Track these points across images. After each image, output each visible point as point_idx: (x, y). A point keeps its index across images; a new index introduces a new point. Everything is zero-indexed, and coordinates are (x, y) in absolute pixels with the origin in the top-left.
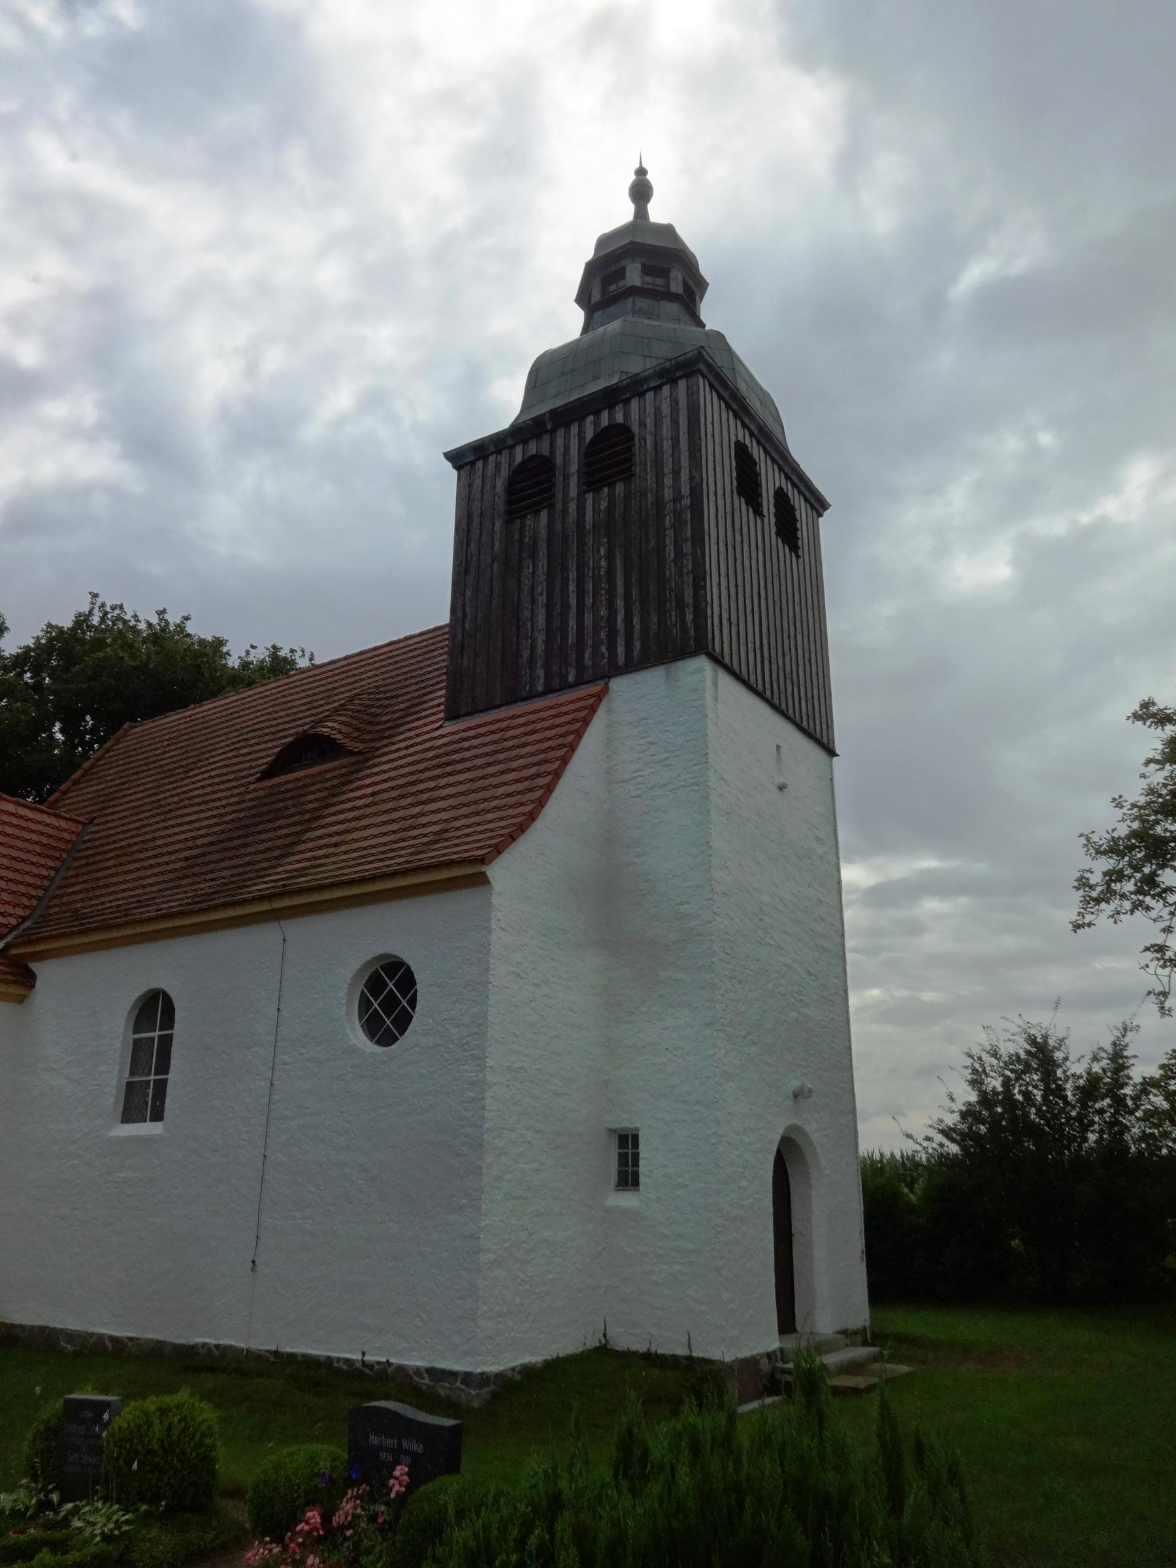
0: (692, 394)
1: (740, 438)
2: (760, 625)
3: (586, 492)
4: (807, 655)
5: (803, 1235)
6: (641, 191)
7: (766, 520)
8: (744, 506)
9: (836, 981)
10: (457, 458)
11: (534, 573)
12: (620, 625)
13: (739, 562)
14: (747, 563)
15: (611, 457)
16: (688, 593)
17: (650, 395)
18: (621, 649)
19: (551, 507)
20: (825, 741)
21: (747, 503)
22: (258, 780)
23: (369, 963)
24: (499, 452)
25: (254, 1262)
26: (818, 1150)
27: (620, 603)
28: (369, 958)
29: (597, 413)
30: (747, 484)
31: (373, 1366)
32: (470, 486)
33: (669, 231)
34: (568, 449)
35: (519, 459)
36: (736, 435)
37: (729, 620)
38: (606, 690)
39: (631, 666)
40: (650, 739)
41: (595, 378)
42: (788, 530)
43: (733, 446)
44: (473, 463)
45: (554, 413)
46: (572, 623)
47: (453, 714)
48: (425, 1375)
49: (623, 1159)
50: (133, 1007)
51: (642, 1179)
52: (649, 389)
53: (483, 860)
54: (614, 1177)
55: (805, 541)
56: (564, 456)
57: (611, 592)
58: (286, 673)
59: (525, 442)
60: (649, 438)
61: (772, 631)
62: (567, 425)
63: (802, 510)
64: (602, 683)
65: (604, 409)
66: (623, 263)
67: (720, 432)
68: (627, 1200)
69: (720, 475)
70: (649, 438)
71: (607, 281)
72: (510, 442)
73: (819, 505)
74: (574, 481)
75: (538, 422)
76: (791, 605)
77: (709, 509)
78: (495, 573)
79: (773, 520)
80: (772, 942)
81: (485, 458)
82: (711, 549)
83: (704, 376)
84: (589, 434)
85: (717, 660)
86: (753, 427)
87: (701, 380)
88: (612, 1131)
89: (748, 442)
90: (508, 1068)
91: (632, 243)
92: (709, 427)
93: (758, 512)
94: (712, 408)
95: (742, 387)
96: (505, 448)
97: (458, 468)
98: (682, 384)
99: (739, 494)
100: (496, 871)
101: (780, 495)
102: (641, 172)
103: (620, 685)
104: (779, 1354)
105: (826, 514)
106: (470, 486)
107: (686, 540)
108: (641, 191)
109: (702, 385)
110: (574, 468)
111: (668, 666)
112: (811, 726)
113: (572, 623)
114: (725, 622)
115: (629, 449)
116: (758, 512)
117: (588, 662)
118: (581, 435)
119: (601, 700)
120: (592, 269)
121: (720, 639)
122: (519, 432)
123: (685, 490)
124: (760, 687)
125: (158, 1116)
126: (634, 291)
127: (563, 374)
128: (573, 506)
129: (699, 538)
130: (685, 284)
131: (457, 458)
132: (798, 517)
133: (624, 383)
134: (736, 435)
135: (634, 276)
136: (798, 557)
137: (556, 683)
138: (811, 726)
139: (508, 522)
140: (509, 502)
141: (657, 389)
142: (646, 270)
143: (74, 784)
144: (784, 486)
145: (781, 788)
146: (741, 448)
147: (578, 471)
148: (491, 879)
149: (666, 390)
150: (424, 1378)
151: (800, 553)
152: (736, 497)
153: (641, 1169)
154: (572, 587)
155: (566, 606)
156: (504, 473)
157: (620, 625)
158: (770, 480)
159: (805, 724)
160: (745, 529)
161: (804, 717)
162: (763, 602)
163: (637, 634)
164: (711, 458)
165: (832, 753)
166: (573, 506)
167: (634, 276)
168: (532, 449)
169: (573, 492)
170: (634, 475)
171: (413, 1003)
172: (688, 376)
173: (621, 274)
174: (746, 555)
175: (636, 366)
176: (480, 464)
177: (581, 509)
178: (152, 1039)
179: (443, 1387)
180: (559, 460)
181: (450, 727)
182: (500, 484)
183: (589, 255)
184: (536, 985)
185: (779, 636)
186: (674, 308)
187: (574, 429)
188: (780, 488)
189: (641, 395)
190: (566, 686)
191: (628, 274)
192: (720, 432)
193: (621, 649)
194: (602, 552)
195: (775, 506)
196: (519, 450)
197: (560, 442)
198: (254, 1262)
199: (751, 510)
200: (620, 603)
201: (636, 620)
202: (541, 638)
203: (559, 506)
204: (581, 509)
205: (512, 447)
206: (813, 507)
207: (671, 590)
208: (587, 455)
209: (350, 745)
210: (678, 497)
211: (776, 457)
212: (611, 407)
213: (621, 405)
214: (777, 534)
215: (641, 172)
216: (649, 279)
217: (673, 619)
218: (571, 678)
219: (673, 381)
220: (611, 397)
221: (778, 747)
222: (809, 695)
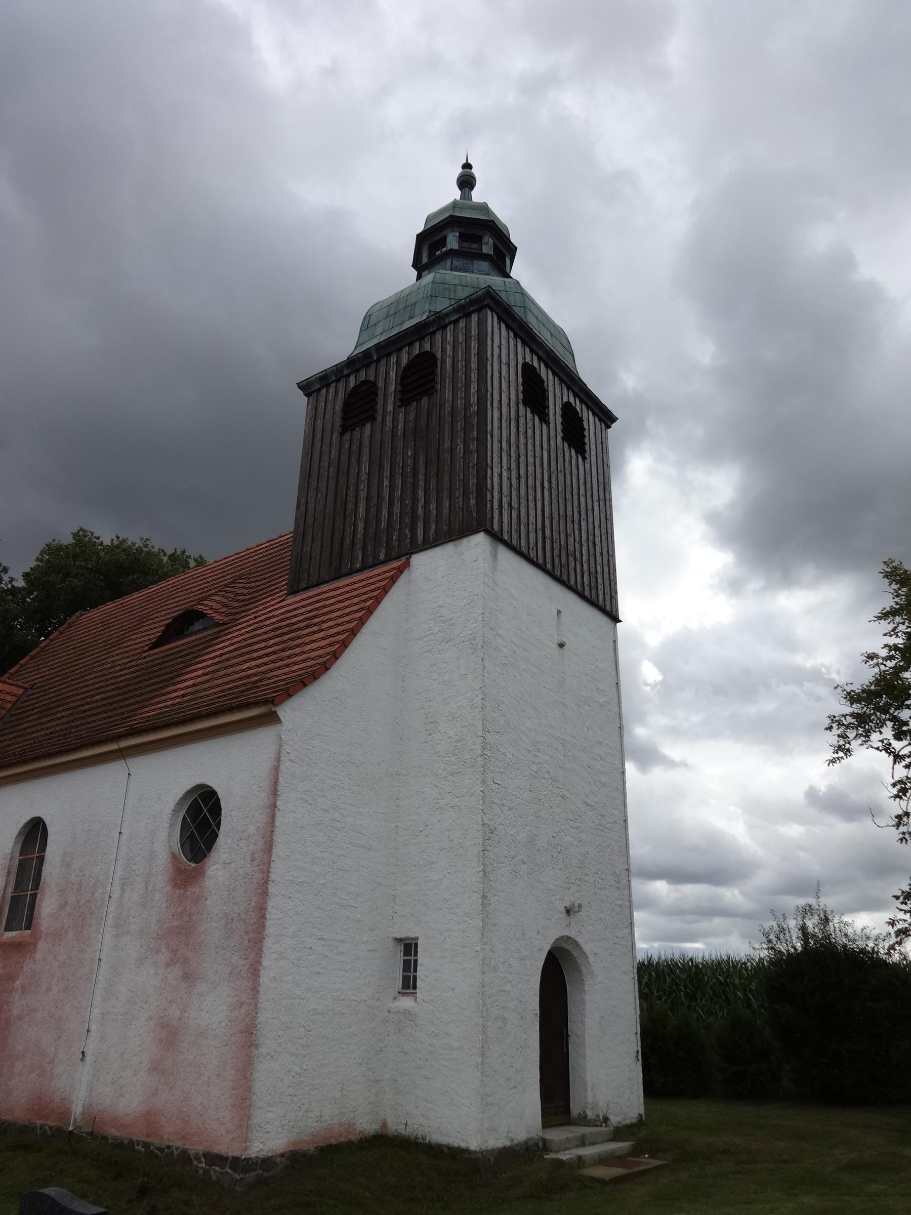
0: (482, 324)
1: (528, 359)
2: (543, 510)
3: (400, 407)
4: (591, 538)
5: (577, 1036)
6: (466, 182)
7: (552, 426)
8: (529, 415)
9: (616, 812)
10: (307, 387)
11: (358, 474)
12: (420, 511)
13: (522, 458)
14: (531, 460)
15: (420, 378)
16: (473, 481)
17: (450, 328)
18: (420, 532)
19: (373, 419)
20: (608, 608)
21: (533, 412)
22: (150, 649)
23: (189, 793)
24: (338, 381)
25: (83, 1053)
26: (591, 959)
27: (421, 493)
28: (189, 788)
29: (411, 344)
30: (534, 396)
31: (164, 1149)
32: (316, 408)
33: (484, 208)
34: (388, 377)
35: (352, 384)
36: (524, 358)
37: (510, 505)
38: (407, 564)
39: (429, 544)
40: (440, 603)
41: (411, 318)
42: (574, 435)
43: (520, 367)
44: (319, 390)
45: (378, 347)
46: (385, 512)
47: (293, 591)
48: (203, 1159)
49: (407, 964)
50: (20, 833)
51: (419, 983)
52: (450, 323)
53: (273, 702)
54: (399, 984)
55: (593, 447)
56: (385, 380)
57: (415, 485)
58: (186, 566)
59: (357, 371)
60: (449, 361)
61: (555, 516)
62: (389, 355)
63: (590, 422)
64: (404, 559)
65: (416, 341)
66: (445, 233)
67: (505, 355)
68: (406, 1003)
69: (505, 387)
70: (449, 361)
71: (434, 247)
72: (346, 372)
73: (607, 418)
74: (391, 399)
75: (367, 354)
76: (575, 497)
77: (494, 415)
78: (331, 475)
79: (559, 427)
80: (547, 776)
81: (328, 386)
82: (493, 446)
83: (492, 310)
84: (405, 361)
85: (496, 537)
86: (540, 353)
87: (489, 313)
88: (399, 940)
89: (536, 364)
90: (292, 882)
91: (451, 216)
92: (496, 351)
93: (544, 419)
94: (499, 338)
95: (532, 322)
96: (343, 377)
97: (308, 395)
98: (474, 318)
99: (525, 404)
100: (285, 711)
101: (567, 408)
102: (467, 166)
103: (418, 560)
104: (541, 1144)
105: (614, 425)
106: (316, 408)
107: (473, 440)
108: (466, 182)
109: (491, 319)
110: (392, 388)
111: (458, 542)
112: (594, 595)
113: (385, 512)
114: (505, 506)
115: (433, 373)
116: (544, 419)
117: (395, 543)
118: (398, 363)
119: (401, 573)
120: (421, 238)
121: (503, 520)
122: (353, 364)
123: (474, 399)
124: (541, 561)
125: (28, 927)
126: (452, 252)
127: (388, 316)
128: (389, 418)
129: (482, 441)
130: (495, 247)
131: (307, 387)
132: (586, 426)
133: (431, 319)
134: (524, 358)
135: (453, 242)
136: (584, 458)
137: (370, 560)
138: (594, 595)
139: (342, 434)
140: (344, 419)
141: (456, 322)
142: (462, 238)
143: (32, 659)
144: (572, 400)
145: (561, 645)
146: (528, 371)
147: (395, 391)
148: (282, 719)
149: (462, 323)
150: (201, 1162)
151: (587, 455)
152: (521, 407)
153: (418, 974)
154: (386, 483)
155: (380, 497)
156: (341, 396)
157: (420, 511)
158: (557, 396)
159: (587, 593)
160: (530, 433)
161: (587, 588)
162: (546, 493)
163: (433, 519)
164: (496, 374)
165: (616, 620)
166: (389, 418)
167: (453, 242)
168: (362, 376)
169: (390, 408)
170: (436, 390)
171: (218, 825)
172: (479, 310)
173: (443, 242)
174: (530, 454)
175: (442, 305)
176: (324, 391)
177: (395, 421)
178: (33, 859)
179: (215, 1171)
180: (381, 383)
181: (291, 599)
182: (338, 407)
183: (420, 228)
184: (325, 811)
185: (562, 521)
186: (485, 265)
187: (393, 359)
188: (568, 403)
189: (444, 327)
190: (377, 563)
191: (448, 242)
192: (505, 355)
193: (420, 532)
194: (410, 453)
195: (562, 416)
196: (352, 378)
197: (382, 369)
198: (83, 1053)
199: (537, 419)
200: (421, 493)
201: (432, 507)
202: (361, 525)
203: (379, 419)
204: (395, 421)
205: (348, 376)
206: (601, 420)
207: (459, 480)
208: (403, 378)
209: (218, 617)
210: (467, 406)
211: (565, 378)
212: (421, 339)
213: (429, 337)
214: (563, 439)
215: (467, 166)
216: (465, 244)
217: (461, 504)
218: (382, 557)
219: (468, 315)
220: (420, 331)
221: (559, 612)
222: (593, 570)
